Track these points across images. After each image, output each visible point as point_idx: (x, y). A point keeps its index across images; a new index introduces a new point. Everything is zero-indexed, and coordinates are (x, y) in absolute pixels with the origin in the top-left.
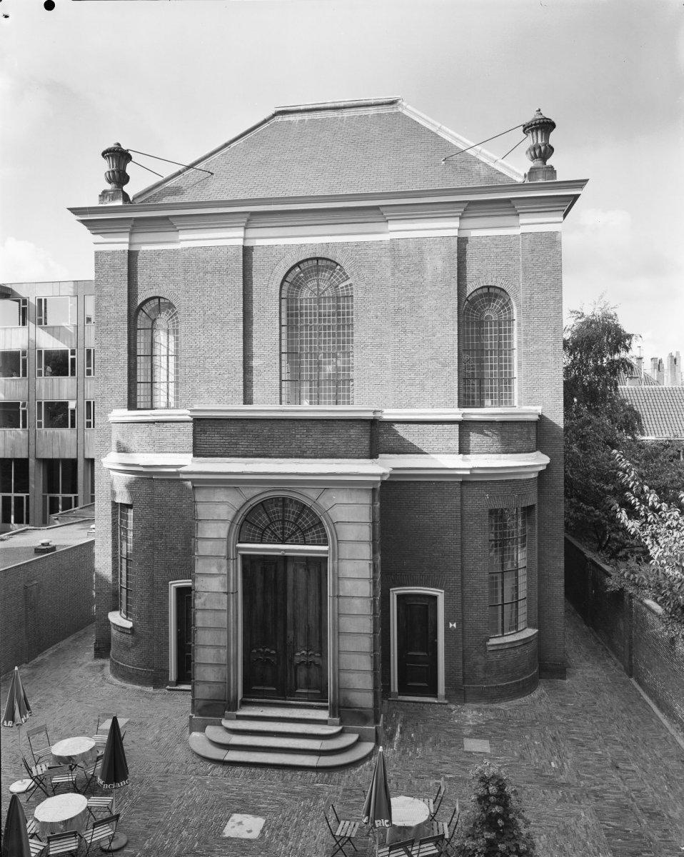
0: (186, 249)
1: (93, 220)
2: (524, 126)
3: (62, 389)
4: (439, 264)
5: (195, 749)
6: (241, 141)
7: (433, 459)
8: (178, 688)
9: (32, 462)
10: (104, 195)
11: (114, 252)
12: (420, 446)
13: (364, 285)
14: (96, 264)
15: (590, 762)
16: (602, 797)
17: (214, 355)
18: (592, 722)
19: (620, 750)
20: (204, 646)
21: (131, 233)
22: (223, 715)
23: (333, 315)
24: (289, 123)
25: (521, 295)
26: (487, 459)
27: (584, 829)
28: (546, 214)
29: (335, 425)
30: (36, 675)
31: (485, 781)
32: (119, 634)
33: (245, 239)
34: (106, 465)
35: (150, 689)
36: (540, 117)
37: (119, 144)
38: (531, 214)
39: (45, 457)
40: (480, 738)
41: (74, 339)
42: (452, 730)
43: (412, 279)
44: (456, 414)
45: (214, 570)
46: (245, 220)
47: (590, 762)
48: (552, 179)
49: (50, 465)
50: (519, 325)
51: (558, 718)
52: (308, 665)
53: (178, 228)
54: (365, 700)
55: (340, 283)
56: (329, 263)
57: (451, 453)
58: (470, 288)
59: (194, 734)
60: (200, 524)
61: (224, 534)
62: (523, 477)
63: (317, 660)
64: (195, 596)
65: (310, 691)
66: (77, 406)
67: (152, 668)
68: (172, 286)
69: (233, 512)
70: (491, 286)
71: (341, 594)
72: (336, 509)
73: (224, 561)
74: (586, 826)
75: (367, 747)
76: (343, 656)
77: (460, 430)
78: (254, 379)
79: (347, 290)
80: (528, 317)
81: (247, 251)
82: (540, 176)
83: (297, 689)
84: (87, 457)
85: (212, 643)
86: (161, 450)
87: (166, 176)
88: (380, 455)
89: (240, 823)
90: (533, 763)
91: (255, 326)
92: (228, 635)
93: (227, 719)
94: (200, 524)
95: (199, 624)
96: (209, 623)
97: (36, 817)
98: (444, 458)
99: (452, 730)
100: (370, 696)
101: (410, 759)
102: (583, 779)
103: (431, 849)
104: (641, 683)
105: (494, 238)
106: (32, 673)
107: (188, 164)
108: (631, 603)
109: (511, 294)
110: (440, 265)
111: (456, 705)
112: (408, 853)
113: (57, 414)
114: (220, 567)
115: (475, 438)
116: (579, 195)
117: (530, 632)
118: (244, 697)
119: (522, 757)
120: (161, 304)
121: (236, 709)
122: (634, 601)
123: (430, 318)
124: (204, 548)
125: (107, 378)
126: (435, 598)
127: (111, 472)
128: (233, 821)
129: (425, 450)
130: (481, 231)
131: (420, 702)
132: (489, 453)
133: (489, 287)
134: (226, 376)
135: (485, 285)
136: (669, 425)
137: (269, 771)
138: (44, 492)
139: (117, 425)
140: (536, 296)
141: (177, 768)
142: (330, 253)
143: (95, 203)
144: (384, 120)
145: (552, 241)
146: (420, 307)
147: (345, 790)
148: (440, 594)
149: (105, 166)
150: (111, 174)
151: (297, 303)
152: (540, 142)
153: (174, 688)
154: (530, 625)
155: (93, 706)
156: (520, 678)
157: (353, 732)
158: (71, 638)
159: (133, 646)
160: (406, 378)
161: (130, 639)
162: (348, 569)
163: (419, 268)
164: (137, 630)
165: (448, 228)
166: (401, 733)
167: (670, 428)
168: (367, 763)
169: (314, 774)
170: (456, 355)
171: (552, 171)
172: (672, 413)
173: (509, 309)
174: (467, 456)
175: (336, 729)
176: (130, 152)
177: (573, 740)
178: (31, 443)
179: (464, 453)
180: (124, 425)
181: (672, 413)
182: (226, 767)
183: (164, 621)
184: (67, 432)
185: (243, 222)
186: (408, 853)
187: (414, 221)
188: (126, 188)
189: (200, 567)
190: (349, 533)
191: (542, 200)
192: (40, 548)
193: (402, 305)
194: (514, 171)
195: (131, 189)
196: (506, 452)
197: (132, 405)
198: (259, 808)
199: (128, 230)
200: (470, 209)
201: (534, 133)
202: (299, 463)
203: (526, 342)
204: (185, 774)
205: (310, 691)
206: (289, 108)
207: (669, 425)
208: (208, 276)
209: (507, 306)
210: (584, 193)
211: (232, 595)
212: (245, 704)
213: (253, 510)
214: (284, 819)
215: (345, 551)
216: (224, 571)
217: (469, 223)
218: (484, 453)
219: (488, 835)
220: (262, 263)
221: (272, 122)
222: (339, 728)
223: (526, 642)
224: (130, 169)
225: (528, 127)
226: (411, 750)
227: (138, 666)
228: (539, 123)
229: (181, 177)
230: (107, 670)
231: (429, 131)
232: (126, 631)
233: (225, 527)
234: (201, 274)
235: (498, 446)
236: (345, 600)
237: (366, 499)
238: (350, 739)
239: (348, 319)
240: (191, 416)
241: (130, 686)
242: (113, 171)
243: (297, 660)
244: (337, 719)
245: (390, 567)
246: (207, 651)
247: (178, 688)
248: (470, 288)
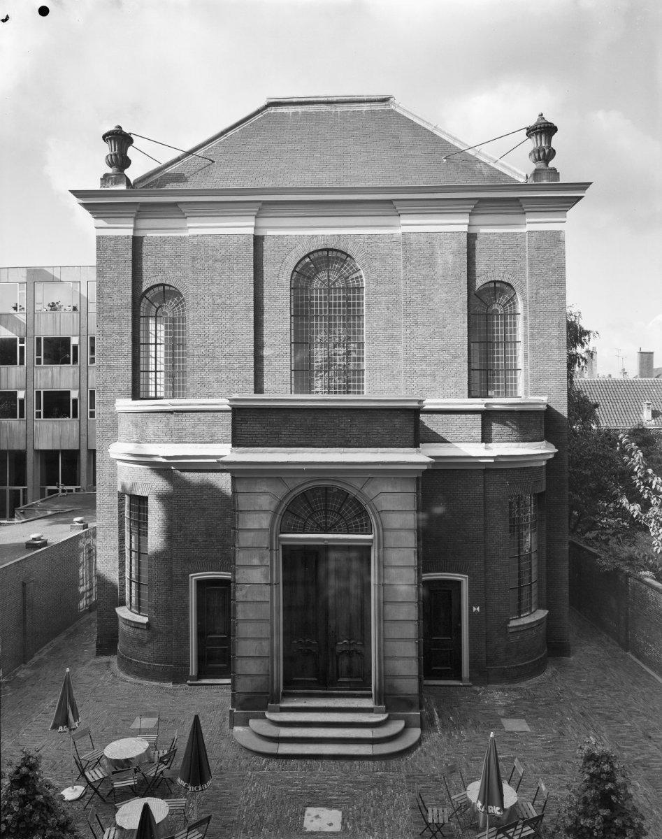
0: (194, 237)
1: (95, 203)
2: (528, 129)
3: (61, 378)
4: (450, 258)
5: (244, 744)
6: (237, 130)
7: (457, 447)
8: (199, 682)
9: (30, 457)
10: (106, 178)
11: (117, 237)
12: (443, 435)
13: (375, 277)
14: (98, 249)
15: (623, 734)
16: (649, 766)
17: (224, 344)
18: (610, 696)
19: (646, 720)
20: (245, 639)
21: (136, 219)
22: (266, 708)
23: (344, 306)
24: (283, 114)
25: (527, 290)
26: (506, 448)
27: (645, 798)
28: (414, 216)
29: (379, 414)
30: (39, 675)
31: (590, 758)
32: (132, 630)
33: (255, 228)
34: (113, 456)
35: (170, 685)
36: (543, 121)
37: (120, 127)
38: (543, 213)
39: (41, 448)
40: (516, 717)
41: (23, 328)
42: (486, 711)
43: (423, 272)
44: (479, 404)
45: (256, 562)
46: (135, 211)
47: (623, 734)
48: (556, 181)
49: (49, 457)
50: (525, 318)
51: (578, 694)
52: (350, 654)
54: (410, 686)
55: (350, 274)
56: (339, 254)
57: (473, 442)
58: (479, 283)
59: (236, 729)
60: (241, 515)
62: (534, 465)
63: (359, 648)
64: (235, 588)
65: (352, 680)
66: (26, 395)
67: (171, 663)
68: (179, 274)
69: (276, 502)
70: (498, 281)
72: (381, 498)
73: (267, 552)
74: (645, 795)
75: (415, 733)
76: (390, 644)
77: (483, 419)
78: (265, 369)
79: (358, 281)
80: (534, 311)
81: (258, 241)
82: (544, 177)
83: (338, 679)
84: (36, 448)
85: (254, 636)
86: (180, 441)
87: (164, 161)
88: (421, 444)
89: (317, 817)
90: (573, 739)
91: (265, 316)
92: (272, 625)
93: (271, 711)
94: (241, 515)
95: (240, 616)
96: (251, 616)
97: (120, 825)
98: (469, 447)
99: (486, 711)
100: (415, 682)
101: (458, 742)
102: (624, 750)
103: (529, 831)
104: (639, 657)
105: (501, 235)
106: (35, 674)
107: (188, 148)
108: (627, 582)
109: (517, 289)
110: (450, 259)
111: (480, 686)
112: (507, 835)
113: (57, 404)
114: (262, 558)
115: (496, 428)
116: (583, 197)
117: (541, 614)
118: (284, 689)
119: (561, 733)
120: (167, 293)
121: (279, 702)
122: (631, 580)
123: (441, 310)
124: (245, 539)
125: (109, 367)
126: (459, 583)
127: (118, 463)
128: (309, 815)
129: (449, 439)
130: (490, 228)
131: (446, 686)
132: (508, 441)
133: (495, 282)
134: (236, 366)
135: (493, 280)
136: (605, 416)
137: (325, 762)
138: (41, 484)
139: (129, 414)
140: (541, 292)
141: (230, 764)
142: (342, 245)
143: (96, 186)
144: (377, 119)
145: (556, 239)
146: (431, 300)
147: (408, 777)
148: (464, 579)
149: (106, 149)
150: (113, 157)
151: (307, 293)
152: (543, 145)
153: (195, 682)
154: (540, 607)
155: (114, 705)
156: (535, 657)
157: (398, 718)
158: (63, 636)
159: (149, 642)
160: (417, 369)
161: (145, 635)
162: (395, 557)
163: (431, 262)
164: (154, 625)
165: (458, 224)
166: (439, 717)
167: (606, 418)
168: (419, 749)
169: (371, 763)
170: (466, 347)
171: (555, 173)
172: (608, 404)
173: (514, 304)
174: (490, 445)
175: (382, 717)
176: (132, 136)
177: (600, 714)
178: (28, 434)
179: (486, 442)
180: (138, 414)
181: (608, 404)
182: (280, 761)
183: (184, 615)
184: (14, 423)
185: (255, 211)
186: (507, 835)
187: (426, 216)
188: (126, 172)
189: (241, 558)
190: (395, 521)
191: (547, 200)
192: (32, 542)
193: (414, 297)
194: (515, 172)
195: (133, 173)
196: (524, 441)
197: (136, 395)
198: (331, 800)
199: (255, 214)
200: (480, 206)
201: (538, 137)
202: (344, 452)
203: (532, 335)
204: (241, 769)
205: (352, 680)
206: (330, 99)
207: (605, 416)
208: (218, 265)
209: (512, 301)
210: (587, 194)
211: (274, 586)
212: (287, 695)
213: (293, 502)
214: (360, 810)
215: (391, 539)
216: (267, 562)
217: (478, 220)
218: (504, 442)
219: (605, 812)
220: (273, 253)
221: (265, 112)
222: (386, 716)
223: (539, 622)
224: (131, 152)
225: (533, 130)
226: (455, 733)
227: (155, 662)
228: (544, 127)
229: (180, 163)
230: (115, 666)
231: (425, 129)
232: (140, 626)
234: (210, 262)
235: (516, 435)
237: (411, 488)
238: (398, 726)
239: (358, 310)
240: (230, 405)
241: (146, 683)
242: (115, 155)
243: (339, 649)
246: (248, 643)
247: (199, 682)
248: (479, 283)
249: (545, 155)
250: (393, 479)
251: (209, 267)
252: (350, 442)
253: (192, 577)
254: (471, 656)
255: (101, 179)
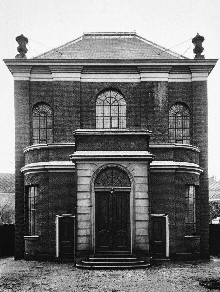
17: (68, 127)
21: (31, 73)
45: (85, 197)
53: (52, 72)
61: (88, 182)
69: (93, 173)
71: (136, 205)
85: (84, 227)
114: (87, 196)
149: (17, 45)
213: (101, 172)
233: (89, 180)
236: (139, 208)
244: (135, 255)
245: (154, 204)
249: (198, 50)
250: (139, 163)
251: (62, 94)
252: (122, 149)
253: (57, 216)
254: (170, 242)
255: (16, 56)
